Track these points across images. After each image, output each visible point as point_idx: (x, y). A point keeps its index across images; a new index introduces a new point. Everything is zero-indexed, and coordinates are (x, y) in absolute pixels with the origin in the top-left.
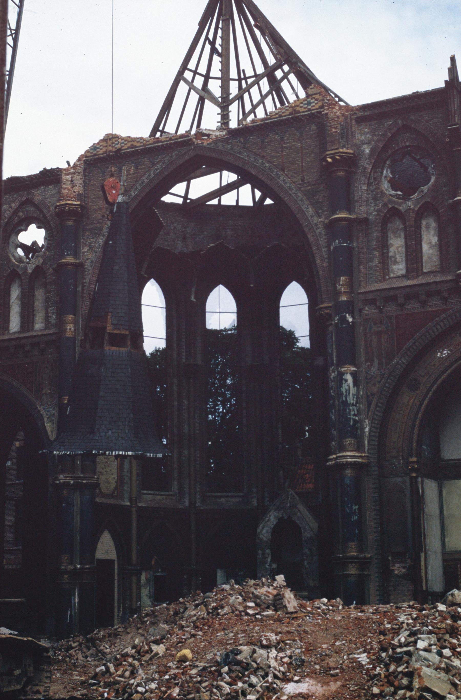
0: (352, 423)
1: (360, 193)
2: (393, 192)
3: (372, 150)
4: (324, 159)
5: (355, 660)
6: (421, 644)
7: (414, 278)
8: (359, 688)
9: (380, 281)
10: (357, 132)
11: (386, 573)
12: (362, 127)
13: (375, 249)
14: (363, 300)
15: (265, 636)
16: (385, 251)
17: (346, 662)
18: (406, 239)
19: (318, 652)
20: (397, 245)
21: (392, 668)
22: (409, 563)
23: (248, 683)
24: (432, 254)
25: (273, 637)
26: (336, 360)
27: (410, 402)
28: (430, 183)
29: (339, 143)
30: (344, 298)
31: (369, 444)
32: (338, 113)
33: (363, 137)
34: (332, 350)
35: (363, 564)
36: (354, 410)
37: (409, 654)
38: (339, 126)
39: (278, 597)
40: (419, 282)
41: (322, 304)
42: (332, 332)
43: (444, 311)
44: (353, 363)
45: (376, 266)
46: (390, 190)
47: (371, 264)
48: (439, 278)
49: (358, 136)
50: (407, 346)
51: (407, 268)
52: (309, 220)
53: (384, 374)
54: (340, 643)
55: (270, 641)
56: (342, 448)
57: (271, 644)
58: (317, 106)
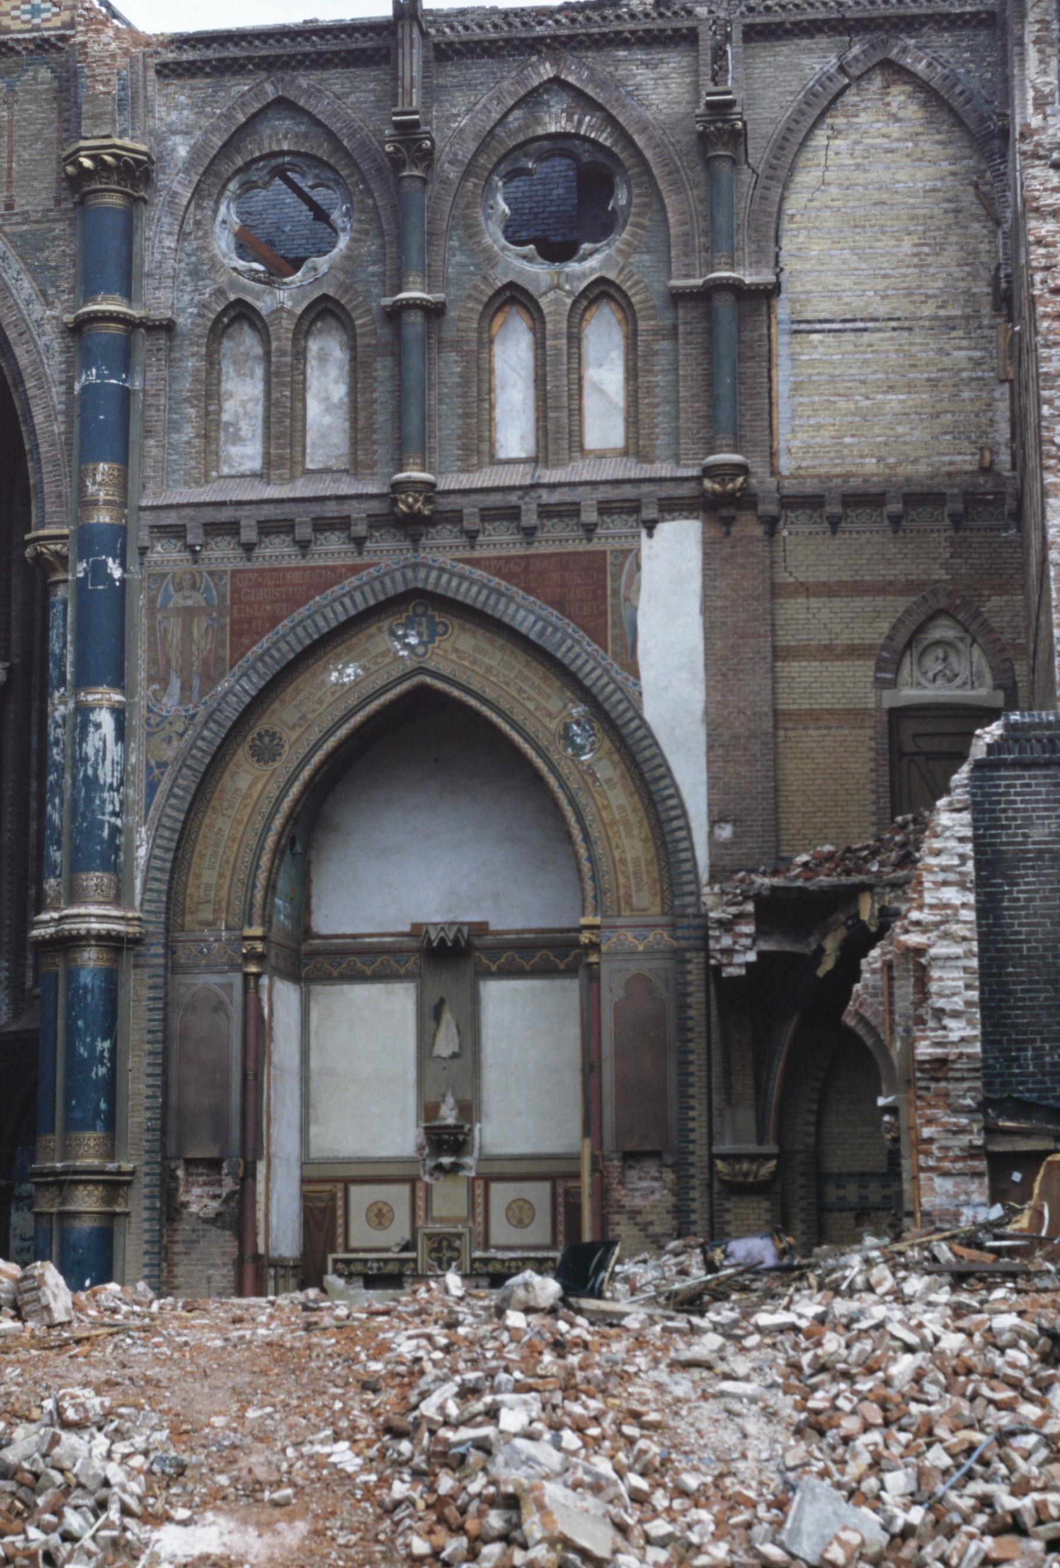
0: (106, 834)
1: (158, 257)
2: (241, 264)
3: (196, 152)
4: (72, 159)
5: (319, 1463)
6: (512, 1420)
7: (283, 481)
8: (362, 1539)
9: (198, 483)
10: (159, 100)
11: (169, 1210)
12: (172, 89)
13: (187, 400)
14: (152, 527)
15: (73, 1397)
16: (212, 408)
17: (299, 1464)
18: (267, 382)
19: (206, 1437)
20: (243, 394)
21: (446, 1483)
22: (229, 1185)
23: (60, 1530)
24: (329, 427)
25: (95, 1403)
26: (74, 674)
27: (257, 791)
28: (336, 250)
29: (114, 121)
30: (103, 517)
31: (145, 890)
32: (113, 46)
33: (174, 116)
34: (64, 646)
35: (115, 1186)
36: (111, 801)
37: (484, 1446)
38: (114, 79)
39: (27, 1284)
40: (298, 494)
41: (43, 527)
42: (65, 603)
43: (354, 570)
44: (118, 681)
45: (188, 443)
46: (234, 256)
47: (175, 436)
48: (347, 487)
49: (160, 111)
50: (257, 649)
51: (267, 454)
52: (20, 311)
53: (193, 716)
54: (259, 1413)
55: (86, 1410)
56: (74, 896)
57: (87, 1418)
58: (57, 22)
